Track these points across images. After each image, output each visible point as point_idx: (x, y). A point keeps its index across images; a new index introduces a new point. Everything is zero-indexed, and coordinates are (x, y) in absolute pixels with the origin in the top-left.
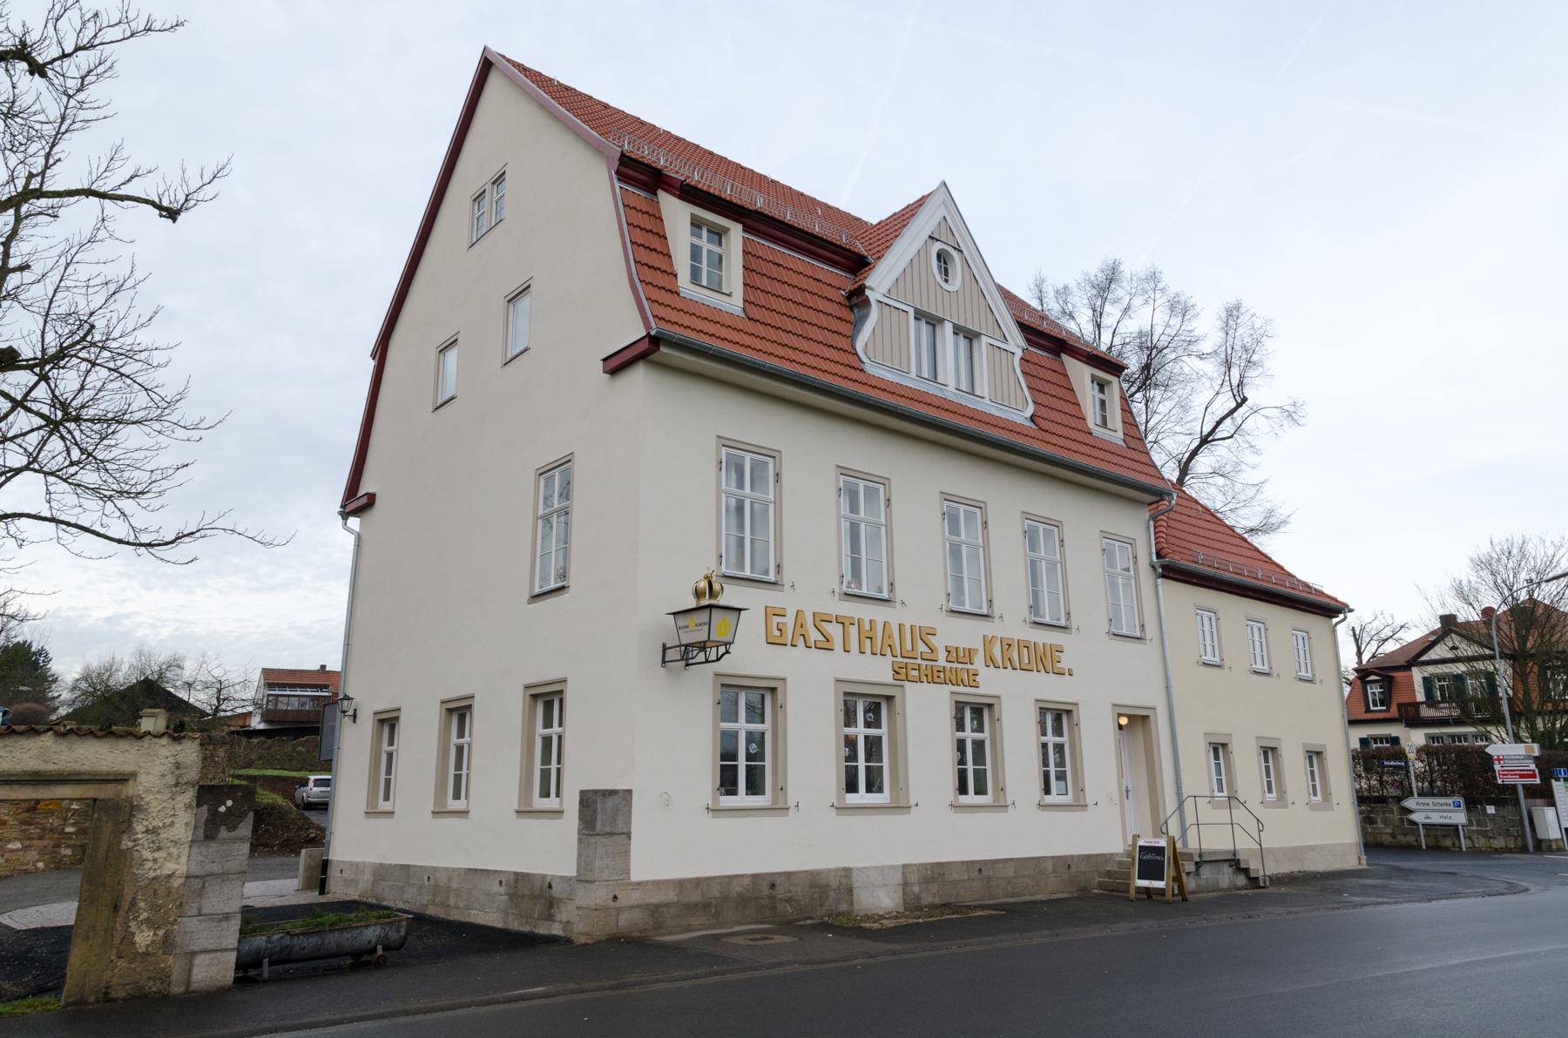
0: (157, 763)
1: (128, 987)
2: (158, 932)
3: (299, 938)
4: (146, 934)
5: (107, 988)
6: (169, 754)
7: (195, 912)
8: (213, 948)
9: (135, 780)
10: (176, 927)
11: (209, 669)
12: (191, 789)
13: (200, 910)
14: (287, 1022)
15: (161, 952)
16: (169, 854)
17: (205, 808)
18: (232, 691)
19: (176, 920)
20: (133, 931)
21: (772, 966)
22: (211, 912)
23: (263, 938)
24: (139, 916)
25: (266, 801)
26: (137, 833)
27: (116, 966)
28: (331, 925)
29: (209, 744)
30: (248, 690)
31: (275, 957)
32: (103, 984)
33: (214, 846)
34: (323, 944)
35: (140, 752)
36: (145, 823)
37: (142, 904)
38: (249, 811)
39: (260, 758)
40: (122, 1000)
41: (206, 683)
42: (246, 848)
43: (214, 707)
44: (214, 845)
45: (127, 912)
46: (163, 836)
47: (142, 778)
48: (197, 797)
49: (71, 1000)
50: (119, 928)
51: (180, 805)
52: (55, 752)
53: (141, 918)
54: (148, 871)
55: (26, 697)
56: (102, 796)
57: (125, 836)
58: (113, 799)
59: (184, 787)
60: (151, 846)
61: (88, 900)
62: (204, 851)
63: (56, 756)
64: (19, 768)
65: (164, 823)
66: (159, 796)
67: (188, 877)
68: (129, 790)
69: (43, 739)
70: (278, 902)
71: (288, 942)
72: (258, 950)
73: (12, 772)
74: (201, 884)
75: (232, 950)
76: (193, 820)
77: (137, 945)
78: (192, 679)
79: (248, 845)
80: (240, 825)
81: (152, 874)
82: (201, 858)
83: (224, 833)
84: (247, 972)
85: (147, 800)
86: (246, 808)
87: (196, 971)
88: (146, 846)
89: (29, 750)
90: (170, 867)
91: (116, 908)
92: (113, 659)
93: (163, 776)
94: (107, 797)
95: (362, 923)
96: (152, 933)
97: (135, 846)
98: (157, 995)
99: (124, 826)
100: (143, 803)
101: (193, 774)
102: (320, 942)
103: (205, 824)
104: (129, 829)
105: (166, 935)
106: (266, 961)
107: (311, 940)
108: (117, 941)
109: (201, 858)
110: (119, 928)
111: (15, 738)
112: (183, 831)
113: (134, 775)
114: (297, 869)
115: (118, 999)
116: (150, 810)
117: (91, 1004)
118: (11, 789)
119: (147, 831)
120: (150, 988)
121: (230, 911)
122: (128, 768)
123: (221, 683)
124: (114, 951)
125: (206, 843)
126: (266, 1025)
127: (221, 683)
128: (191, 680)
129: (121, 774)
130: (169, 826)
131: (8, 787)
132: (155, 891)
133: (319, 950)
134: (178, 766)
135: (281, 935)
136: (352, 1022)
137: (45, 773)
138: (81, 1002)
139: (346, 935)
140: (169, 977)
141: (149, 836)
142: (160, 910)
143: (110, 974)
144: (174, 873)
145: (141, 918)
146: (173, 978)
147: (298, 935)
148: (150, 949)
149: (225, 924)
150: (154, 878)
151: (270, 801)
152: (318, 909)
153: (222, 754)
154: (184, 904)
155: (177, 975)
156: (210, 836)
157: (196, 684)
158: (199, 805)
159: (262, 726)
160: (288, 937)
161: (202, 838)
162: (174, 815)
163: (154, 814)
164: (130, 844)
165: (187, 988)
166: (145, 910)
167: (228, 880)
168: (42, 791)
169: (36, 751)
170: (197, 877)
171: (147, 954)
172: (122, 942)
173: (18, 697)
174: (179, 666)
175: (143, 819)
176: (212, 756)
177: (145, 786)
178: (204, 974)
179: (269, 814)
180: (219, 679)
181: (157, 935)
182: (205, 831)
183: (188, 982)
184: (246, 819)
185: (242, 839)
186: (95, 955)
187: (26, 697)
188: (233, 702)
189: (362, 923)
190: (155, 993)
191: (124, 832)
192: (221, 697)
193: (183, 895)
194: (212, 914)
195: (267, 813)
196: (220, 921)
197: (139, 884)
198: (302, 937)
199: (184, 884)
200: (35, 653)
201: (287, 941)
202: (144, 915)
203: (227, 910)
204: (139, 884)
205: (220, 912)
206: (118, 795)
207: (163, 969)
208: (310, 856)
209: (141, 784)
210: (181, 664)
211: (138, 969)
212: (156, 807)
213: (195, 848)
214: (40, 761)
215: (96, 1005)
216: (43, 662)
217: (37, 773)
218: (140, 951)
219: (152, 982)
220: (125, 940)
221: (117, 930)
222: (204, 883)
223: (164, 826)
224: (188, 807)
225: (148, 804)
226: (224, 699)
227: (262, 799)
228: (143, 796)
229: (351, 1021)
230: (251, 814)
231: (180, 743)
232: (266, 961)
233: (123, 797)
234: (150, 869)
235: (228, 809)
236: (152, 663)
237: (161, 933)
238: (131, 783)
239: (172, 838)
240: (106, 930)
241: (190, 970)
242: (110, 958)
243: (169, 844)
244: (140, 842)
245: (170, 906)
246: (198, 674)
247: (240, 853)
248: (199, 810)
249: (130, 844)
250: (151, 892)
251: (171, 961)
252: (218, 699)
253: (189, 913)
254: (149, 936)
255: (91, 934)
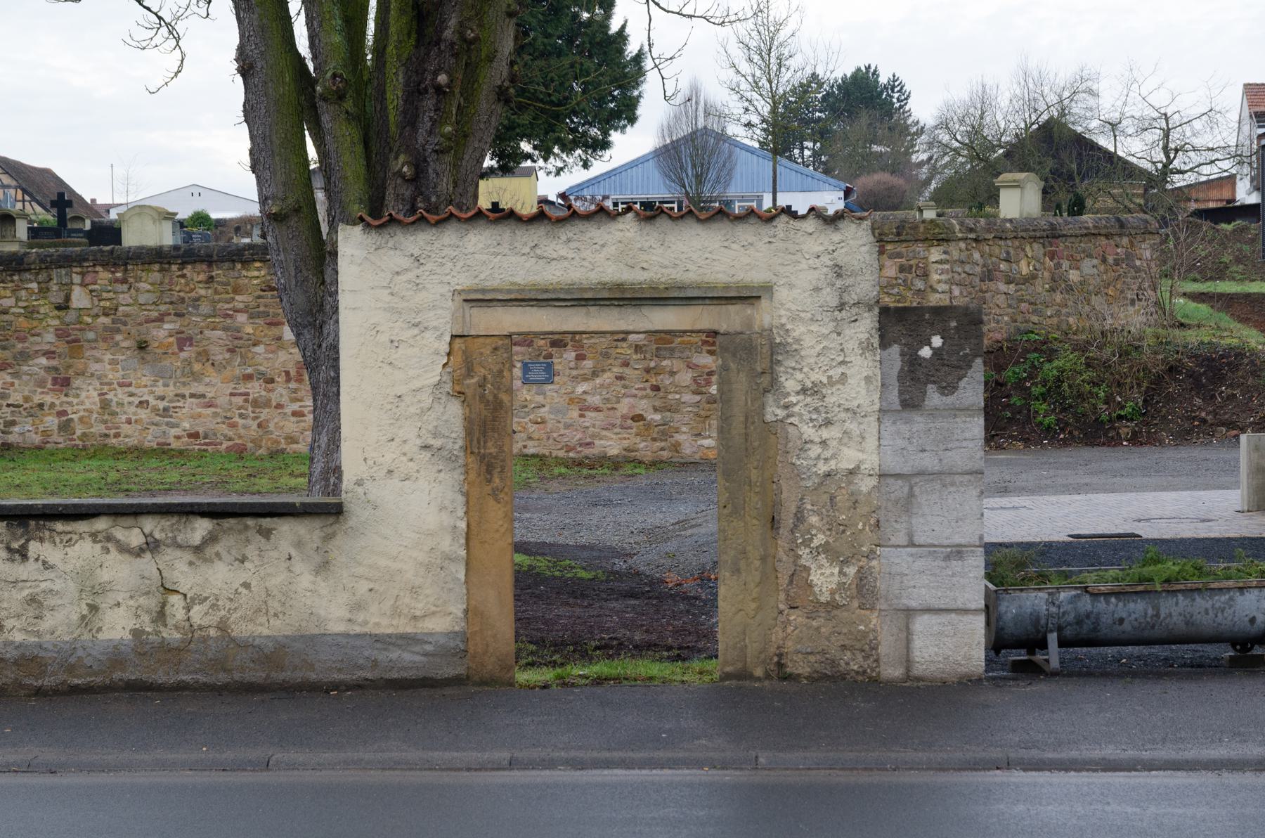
0: (804, 265)
1: (812, 658)
2: (845, 569)
3: (1108, 603)
4: (828, 572)
5: (780, 655)
6: (822, 248)
7: (902, 540)
8: (943, 607)
9: (771, 298)
10: (874, 563)
11: (1144, 93)
12: (866, 315)
13: (910, 535)
14: (1035, 753)
15: (856, 604)
16: (845, 432)
17: (895, 349)
18: (1188, 134)
19: (873, 552)
20: (807, 564)
21: (29, 768)
22: (930, 541)
23: (1041, 594)
24: (811, 540)
25: (1228, 341)
26: (788, 394)
27: (789, 622)
28: (1168, 581)
29: (1121, 235)
30: (1216, 131)
31: (1068, 632)
32: (773, 650)
33: (919, 421)
34: (1158, 615)
35: (772, 246)
36: (799, 376)
37: (814, 519)
38: (976, 356)
39: (1238, 261)
40: (806, 678)
41: (1143, 119)
42: (976, 427)
43: (1160, 166)
44: (919, 419)
45: (792, 532)
46: (830, 400)
47: (782, 294)
48: (880, 330)
49: (728, 669)
50: (785, 558)
51: (851, 345)
52: (641, 249)
53: (816, 543)
54: (816, 462)
55: (879, 162)
56: (723, 328)
57: (770, 398)
58: (741, 333)
59: (854, 310)
60: (814, 416)
61: (729, 506)
62: (904, 428)
63: (644, 257)
64: (594, 277)
65: (830, 377)
66: (814, 327)
67: (882, 476)
68: (763, 316)
69: (621, 226)
70: (1203, 532)
71: (1089, 607)
72: (1035, 619)
73: (585, 284)
74: (906, 490)
75: (976, 611)
76: (878, 372)
77: (816, 589)
78: (1117, 115)
79: (980, 421)
80: (962, 383)
81: (822, 468)
82: (900, 443)
83: (934, 397)
84: (1033, 654)
85: (796, 334)
86: (968, 351)
87: (917, 643)
88: (806, 417)
89: (603, 246)
90: (849, 457)
91: (774, 523)
92: (984, 87)
93: (817, 289)
94: (731, 330)
95: (1230, 583)
96: (836, 570)
97: (788, 416)
98: (860, 678)
99: (765, 381)
100: (790, 340)
101: (866, 287)
102: (1150, 612)
103: (900, 378)
104: (773, 385)
105: (862, 576)
106: (1053, 638)
107: (1132, 606)
108: (783, 580)
109: (900, 443)
110: (785, 558)
111: (579, 226)
112: (864, 392)
113: (768, 289)
114: (1237, 467)
115: (799, 675)
116: (803, 353)
117: (759, 679)
118: (588, 314)
119: (804, 391)
120: (847, 664)
121: (963, 542)
122: (757, 277)
123: (1167, 119)
124: (782, 596)
125: (905, 414)
126: (995, 753)
127: (1167, 119)
128: (1115, 116)
129: (746, 287)
130: (837, 382)
131: (583, 310)
132: (832, 498)
133: (1153, 627)
134: (838, 271)
135: (1073, 593)
136: (1150, 770)
137: (632, 287)
138: (743, 675)
139: (1201, 603)
140: (876, 648)
141: (809, 399)
142: (844, 532)
143: (781, 635)
144: (858, 468)
145: (816, 543)
146: (882, 650)
147: (1107, 595)
148: (837, 597)
149: (956, 565)
150: (828, 475)
151: (1235, 342)
152: (1153, 550)
153: (1148, 254)
154: (881, 524)
155: (887, 646)
156: (910, 403)
157: (1124, 123)
158: (884, 344)
159: (1254, 199)
160: (1088, 596)
161: (897, 406)
162: (843, 363)
163: (812, 360)
164: (781, 413)
165: (908, 669)
166: (819, 530)
167: (953, 484)
168: (632, 317)
169: (613, 248)
170: (897, 476)
171: (832, 606)
172: (791, 582)
173: (868, 163)
174: (1090, 92)
175: (794, 369)
176: (1129, 257)
177: (789, 310)
178: (932, 650)
179: (1234, 367)
180: (1163, 111)
181: (845, 575)
182: (901, 393)
183: (908, 662)
184: (970, 373)
185: (966, 410)
186: (753, 600)
187: (879, 162)
188: (1192, 154)
189: (1230, 583)
190: (857, 673)
191: (766, 391)
192: (1172, 146)
193: (879, 508)
194: (935, 546)
195: (1229, 364)
196: (948, 558)
197: (803, 483)
198: (1113, 600)
199: (877, 488)
200: (886, 88)
201: (1086, 604)
202: (819, 539)
203: (957, 540)
204: (803, 483)
205: (946, 542)
206: (749, 325)
207: (864, 635)
208: (1257, 448)
209: (782, 304)
210: (1094, 87)
211: (823, 630)
212: (813, 347)
213: (887, 423)
214: (622, 265)
215: (767, 683)
216: (898, 100)
217: (620, 286)
218: (823, 599)
219: (848, 654)
220: (795, 578)
221: (780, 561)
222: (911, 488)
223: (831, 382)
224: (866, 347)
225: (798, 341)
226: (1177, 150)
227: (1222, 337)
228: (788, 327)
229: (1150, 766)
230: (979, 362)
231: (837, 229)
232: (1053, 638)
233: (756, 329)
234: (818, 458)
235: (937, 352)
236: (1046, 90)
237: (851, 570)
238: (764, 303)
239: (848, 404)
240: (763, 559)
241: (908, 641)
242: (778, 607)
243: (843, 415)
244: (796, 409)
245: (860, 526)
246: (1125, 103)
247: (967, 435)
248: (886, 353)
249: (781, 413)
250: (826, 498)
251: (874, 621)
252: (1166, 149)
253: (894, 541)
254: (832, 574)
255: (742, 564)
